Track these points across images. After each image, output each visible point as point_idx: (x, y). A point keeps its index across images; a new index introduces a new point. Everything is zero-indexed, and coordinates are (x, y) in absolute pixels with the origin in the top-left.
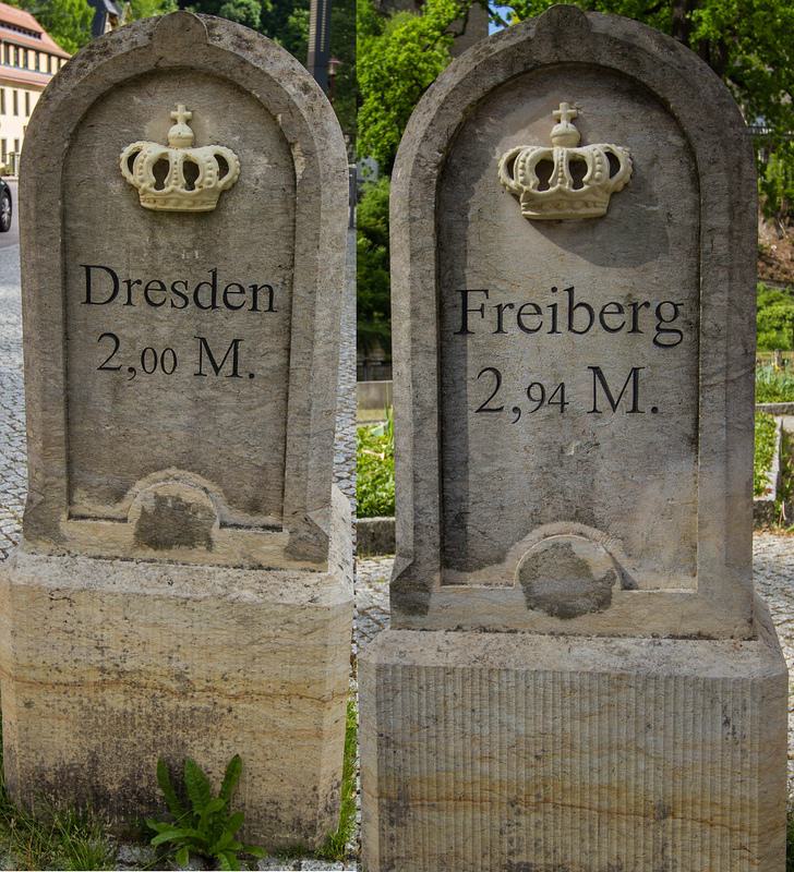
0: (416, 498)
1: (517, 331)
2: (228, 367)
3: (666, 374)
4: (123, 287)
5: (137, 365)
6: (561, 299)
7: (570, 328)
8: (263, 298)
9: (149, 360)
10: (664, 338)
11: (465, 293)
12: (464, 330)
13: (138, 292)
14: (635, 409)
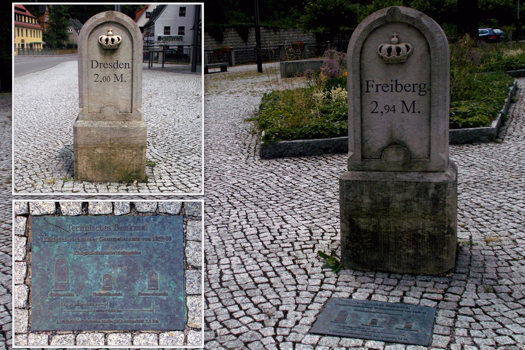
0: (355, 137)
1: (382, 92)
2: (121, 80)
3: (422, 103)
4: (99, 65)
5: (102, 80)
6: (394, 84)
7: (396, 91)
8: (127, 66)
9: (105, 79)
10: (421, 93)
11: (368, 82)
12: (368, 91)
13: (102, 65)
14: (414, 112)
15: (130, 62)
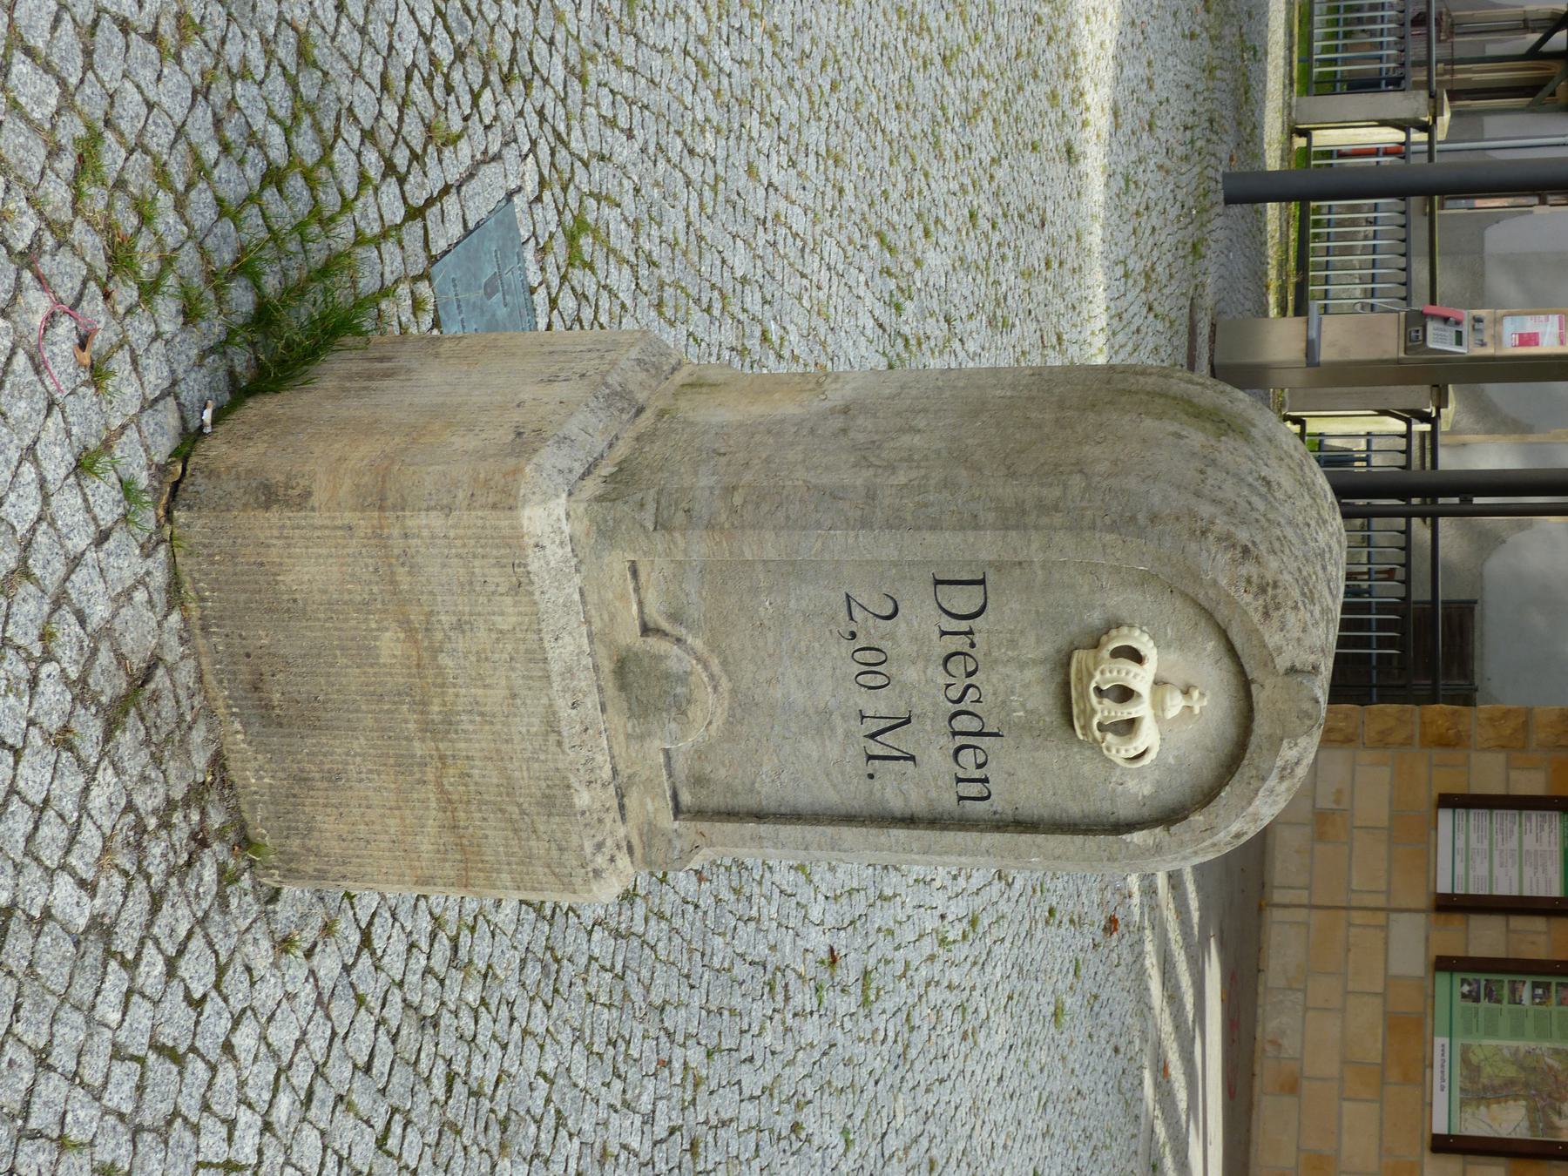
2: (877, 750)
5: (861, 642)
9: (869, 657)
13: (960, 643)
15: (1001, 802)
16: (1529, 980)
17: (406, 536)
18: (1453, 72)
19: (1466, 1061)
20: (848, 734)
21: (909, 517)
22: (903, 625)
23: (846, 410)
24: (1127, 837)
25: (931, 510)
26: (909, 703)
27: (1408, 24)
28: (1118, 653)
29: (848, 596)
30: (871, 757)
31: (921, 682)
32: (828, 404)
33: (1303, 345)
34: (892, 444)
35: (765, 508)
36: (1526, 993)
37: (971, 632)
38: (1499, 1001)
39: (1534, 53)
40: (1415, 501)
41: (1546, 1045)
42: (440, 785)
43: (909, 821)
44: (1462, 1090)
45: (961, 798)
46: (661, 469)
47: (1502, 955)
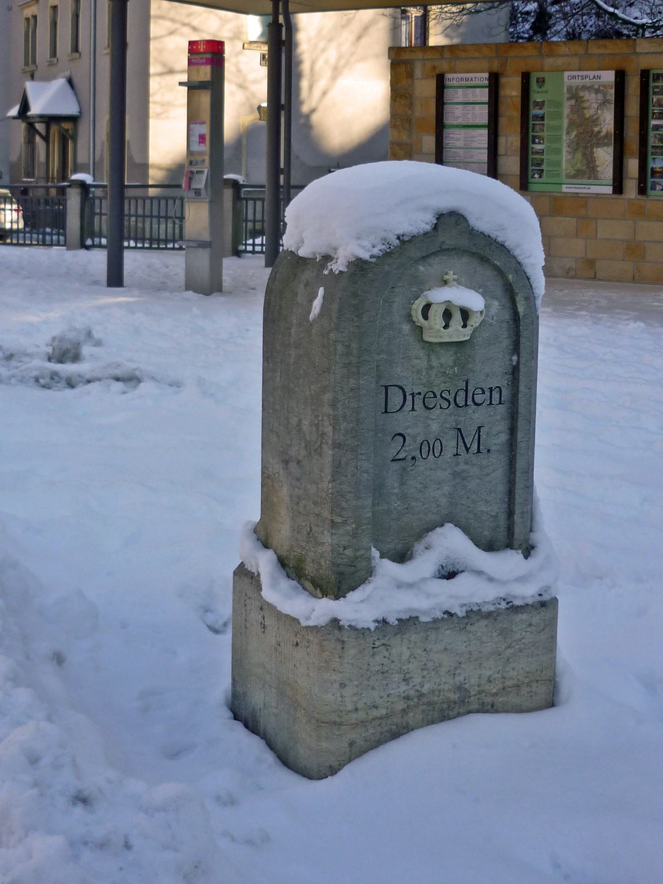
2: (475, 447)
4: (409, 398)
5: (417, 454)
8: (496, 395)
9: (425, 449)
16: (531, 145)
17: (356, 710)
18: (53, 178)
19: (574, 177)
20: (467, 463)
21: (351, 425)
22: (409, 431)
23: (286, 462)
24: (521, 314)
25: (347, 413)
26: (450, 429)
27: (26, 197)
28: (425, 316)
29: (393, 460)
30: (479, 451)
31: (437, 422)
32: (282, 472)
33: (201, 250)
34: (307, 436)
35: (344, 504)
36: (538, 147)
37: (413, 394)
38: (543, 160)
39: (46, 139)
40: (281, 197)
41: (564, 137)
42: (496, 694)
43: (513, 430)
44: (589, 178)
45: (500, 403)
46: (319, 563)
47: (519, 158)
